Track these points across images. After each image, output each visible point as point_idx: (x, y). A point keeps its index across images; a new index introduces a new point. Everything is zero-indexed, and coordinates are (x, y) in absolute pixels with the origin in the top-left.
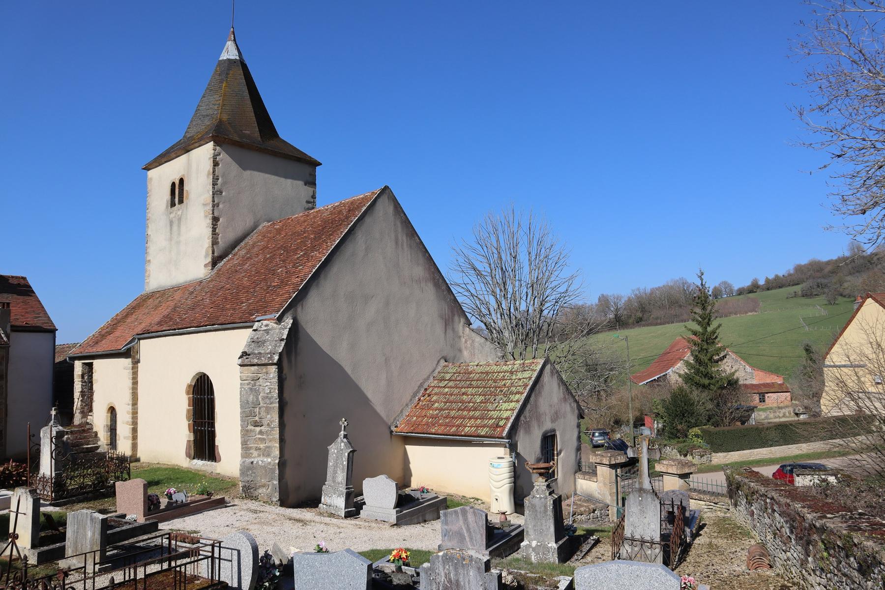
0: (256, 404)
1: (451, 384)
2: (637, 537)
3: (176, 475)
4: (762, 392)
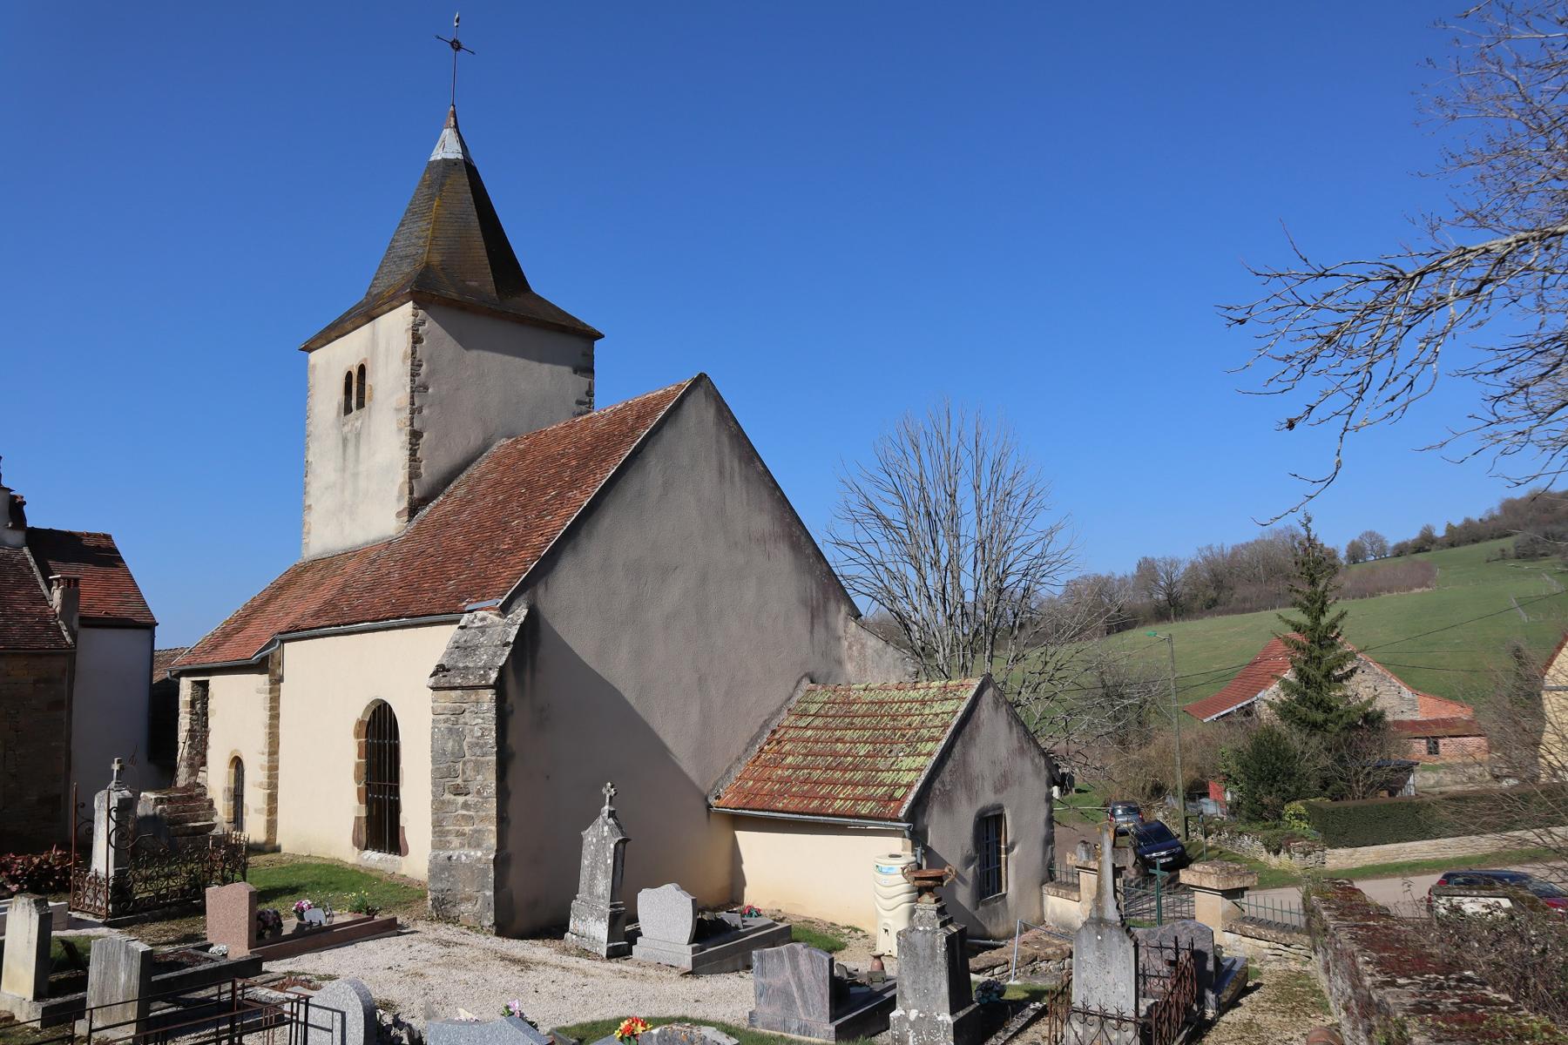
0: (459, 756)
1: (818, 722)
2: (1095, 1008)
3: (329, 878)
4: (1433, 734)
